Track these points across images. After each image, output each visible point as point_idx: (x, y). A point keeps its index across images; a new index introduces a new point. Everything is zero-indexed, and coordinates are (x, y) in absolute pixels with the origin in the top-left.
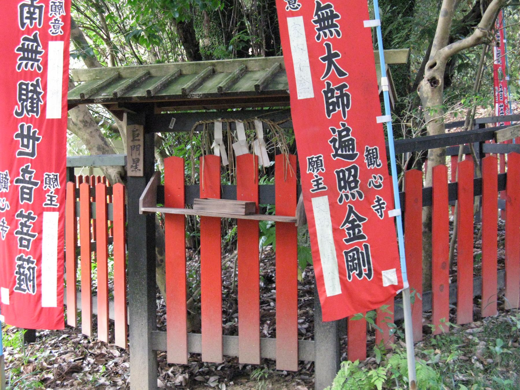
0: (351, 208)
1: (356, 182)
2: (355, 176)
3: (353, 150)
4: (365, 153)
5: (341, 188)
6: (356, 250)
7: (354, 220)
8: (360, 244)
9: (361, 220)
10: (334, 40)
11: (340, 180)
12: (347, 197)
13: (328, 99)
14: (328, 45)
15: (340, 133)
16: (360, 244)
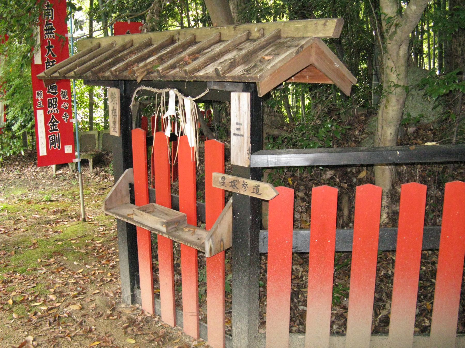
0: (53, 116)
1: (56, 105)
2: (56, 102)
3: (56, 90)
4: (61, 93)
5: (49, 107)
6: (54, 135)
7: (54, 122)
9: (57, 122)
10: (52, 40)
11: (49, 103)
12: (52, 111)
13: (47, 66)
14: (49, 41)
16: (56, 133)
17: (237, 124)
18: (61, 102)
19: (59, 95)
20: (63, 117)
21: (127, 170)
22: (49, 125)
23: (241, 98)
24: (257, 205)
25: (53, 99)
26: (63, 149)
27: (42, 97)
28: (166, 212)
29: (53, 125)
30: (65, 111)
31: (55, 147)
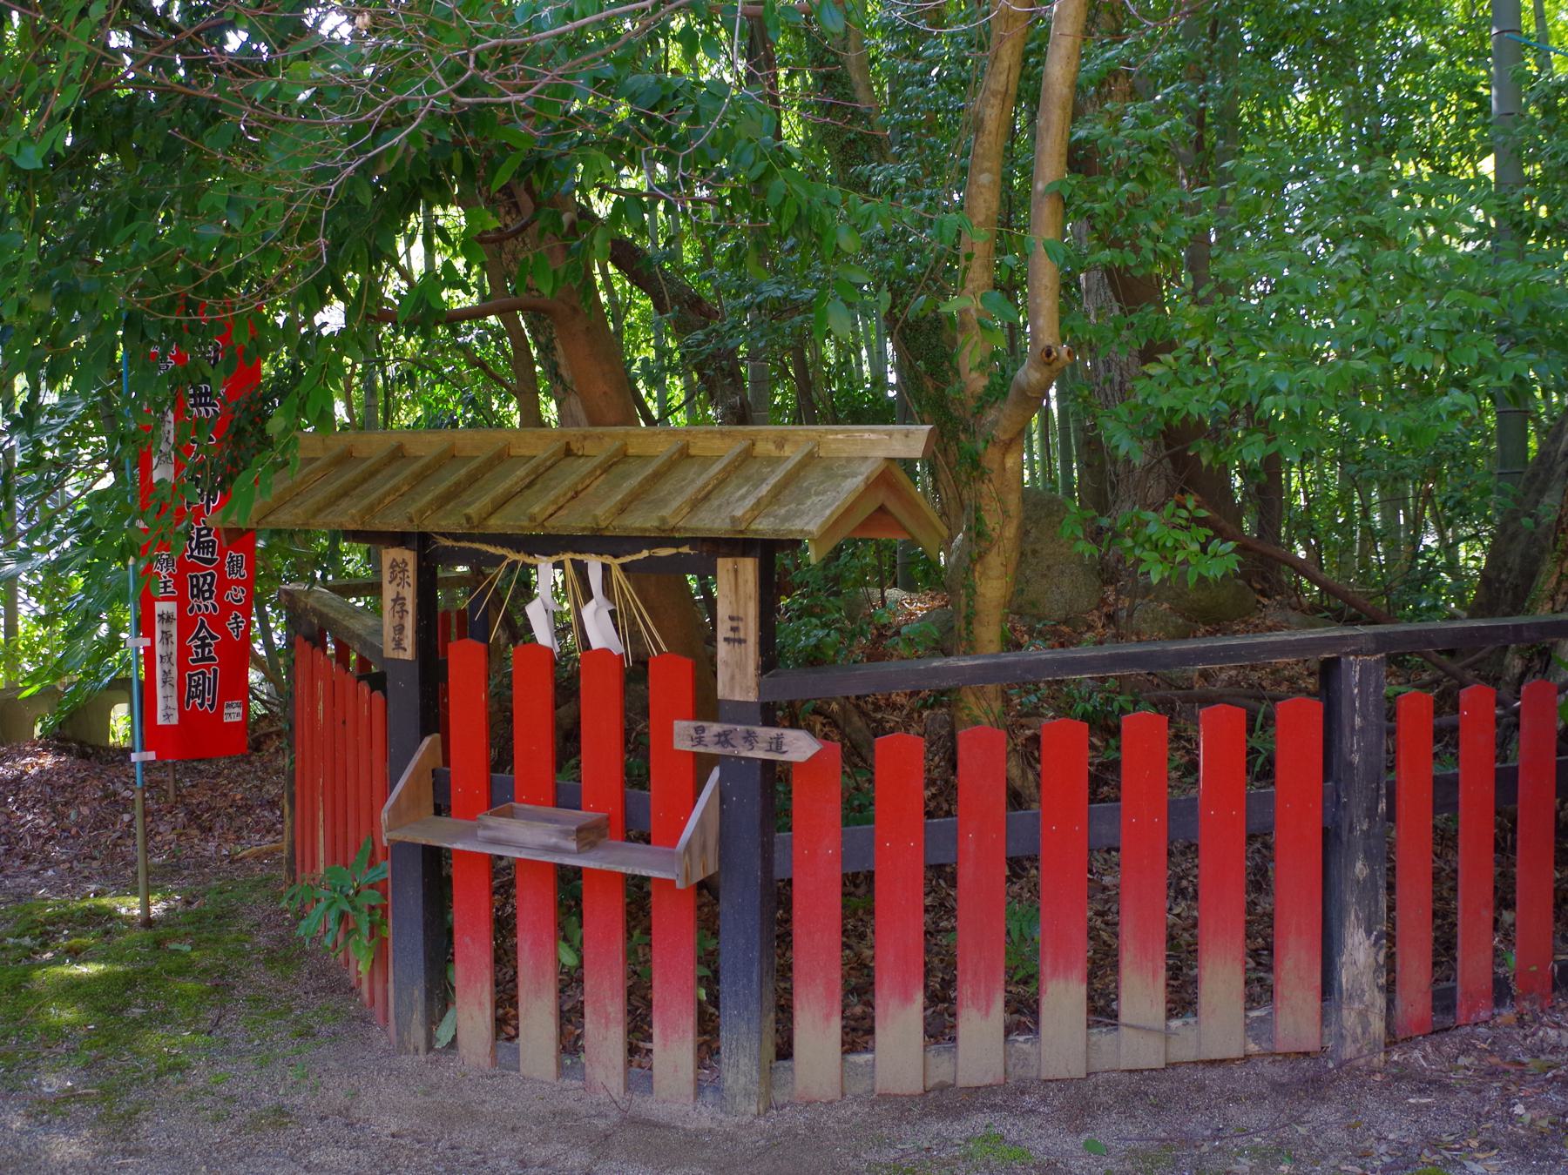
1: (211, 592)
2: (210, 585)
6: (203, 674)
8: (208, 667)
9: (213, 638)
15: (199, 530)
16: (208, 667)
17: (732, 618)
18: (225, 585)
19: (222, 564)
20: (230, 625)
21: (427, 740)
22: (193, 644)
23: (741, 570)
24: (774, 774)
25: (204, 577)
26: (220, 712)
27: (174, 570)
28: (732, 575)
29: (203, 646)
30: (236, 608)
31: (202, 705)
